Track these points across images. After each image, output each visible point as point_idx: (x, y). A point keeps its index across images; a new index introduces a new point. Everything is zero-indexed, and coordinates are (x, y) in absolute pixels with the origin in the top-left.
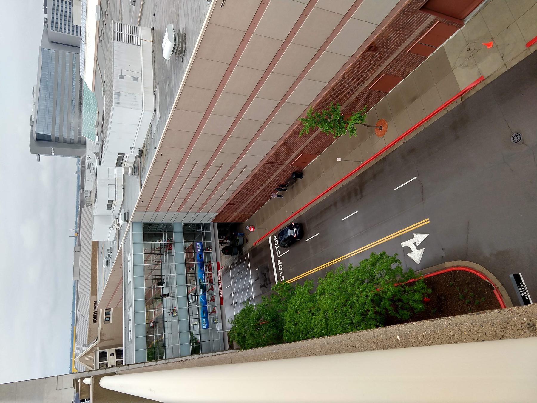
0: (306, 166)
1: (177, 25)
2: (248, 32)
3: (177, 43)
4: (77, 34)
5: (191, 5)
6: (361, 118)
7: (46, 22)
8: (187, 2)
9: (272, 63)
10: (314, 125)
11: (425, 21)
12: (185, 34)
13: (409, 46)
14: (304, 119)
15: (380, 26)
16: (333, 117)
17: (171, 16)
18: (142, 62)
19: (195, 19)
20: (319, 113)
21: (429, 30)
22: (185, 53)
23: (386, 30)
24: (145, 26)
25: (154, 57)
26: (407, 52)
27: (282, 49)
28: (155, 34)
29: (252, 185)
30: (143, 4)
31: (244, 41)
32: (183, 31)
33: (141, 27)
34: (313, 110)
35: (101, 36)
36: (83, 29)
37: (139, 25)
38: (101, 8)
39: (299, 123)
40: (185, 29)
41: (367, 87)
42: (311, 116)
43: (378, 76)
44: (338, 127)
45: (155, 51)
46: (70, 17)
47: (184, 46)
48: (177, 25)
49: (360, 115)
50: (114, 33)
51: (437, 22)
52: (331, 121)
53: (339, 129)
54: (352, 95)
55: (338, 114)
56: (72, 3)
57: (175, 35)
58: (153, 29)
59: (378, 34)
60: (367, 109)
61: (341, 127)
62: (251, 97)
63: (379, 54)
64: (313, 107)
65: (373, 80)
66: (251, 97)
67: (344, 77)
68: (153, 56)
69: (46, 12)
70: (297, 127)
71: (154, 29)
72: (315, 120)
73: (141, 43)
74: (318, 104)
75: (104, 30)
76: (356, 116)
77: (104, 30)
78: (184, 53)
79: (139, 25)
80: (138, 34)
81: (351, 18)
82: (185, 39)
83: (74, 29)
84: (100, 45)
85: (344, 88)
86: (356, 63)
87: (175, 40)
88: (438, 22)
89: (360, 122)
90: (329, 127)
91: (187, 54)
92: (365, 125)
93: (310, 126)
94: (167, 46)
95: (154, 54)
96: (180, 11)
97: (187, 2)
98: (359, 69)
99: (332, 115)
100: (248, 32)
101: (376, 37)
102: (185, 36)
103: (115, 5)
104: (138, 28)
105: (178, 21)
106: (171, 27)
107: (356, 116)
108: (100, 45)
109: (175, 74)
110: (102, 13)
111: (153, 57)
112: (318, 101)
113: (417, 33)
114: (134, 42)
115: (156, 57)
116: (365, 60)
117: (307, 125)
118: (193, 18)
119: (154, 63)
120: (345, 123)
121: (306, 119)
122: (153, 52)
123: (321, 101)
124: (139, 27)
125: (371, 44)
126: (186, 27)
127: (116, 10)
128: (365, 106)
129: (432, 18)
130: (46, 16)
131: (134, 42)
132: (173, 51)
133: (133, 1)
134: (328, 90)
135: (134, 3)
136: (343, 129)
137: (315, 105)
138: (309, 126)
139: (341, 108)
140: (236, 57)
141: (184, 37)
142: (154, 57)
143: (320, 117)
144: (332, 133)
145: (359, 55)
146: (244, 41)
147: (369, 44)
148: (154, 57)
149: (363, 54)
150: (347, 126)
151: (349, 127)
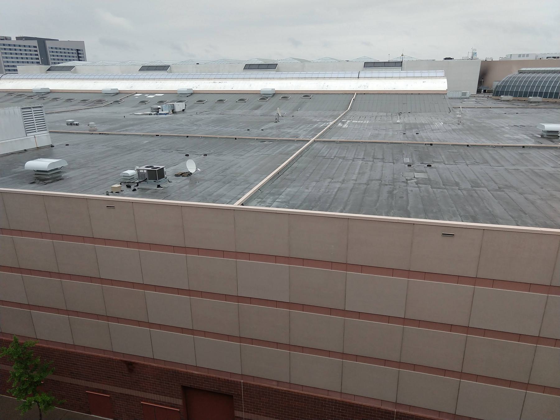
0: (93, 414)
1: (69, 169)
2: (93, 240)
3: (49, 173)
4: (6, 70)
5: (95, 178)
6: (48, 405)
7: (6, 38)
8: (96, 173)
9: (71, 276)
10: (14, 357)
11: (143, 392)
12: (63, 179)
13: (147, 400)
14: (17, 342)
15: (197, 368)
16: (35, 373)
17: (75, 161)
18: (7, 141)
19: (83, 184)
20: (32, 355)
21: (169, 407)
22: (41, 184)
23: (152, 367)
24: (51, 137)
25: (20, 153)
26: (141, 402)
27: (91, 279)
28: (48, 150)
29: (45, 360)
30: (74, 133)
31: (84, 239)
32: (66, 176)
33: (49, 134)
34: (34, 346)
35: (17, 95)
36: (13, 76)
37: (50, 132)
38: (49, 93)
39: (7, 339)
40: (68, 177)
41: (87, 388)
42: (25, 348)
43: (105, 392)
44: (24, 387)
45: (27, 152)
46: (23, 62)
47: (50, 181)
48: (69, 169)
49: (51, 402)
50: (29, 108)
51: (177, 409)
52: (28, 374)
53: (23, 389)
54: (71, 378)
55: (41, 377)
56: (39, 64)
57: (57, 169)
58: (52, 146)
59: (145, 363)
60: (63, 405)
61: (26, 389)
62: (20, 270)
63: (128, 376)
64: (37, 344)
65: (98, 389)
66: (20, 270)
67: (89, 356)
68: (22, 151)
69: (18, 38)
70: (2, 340)
71: (53, 148)
72: (22, 355)
73: (31, 136)
74: (43, 348)
75: (25, 97)
76: (48, 398)
77: (25, 97)
78: (41, 183)
79: (50, 132)
80: (39, 132)
81: (193, 336)
82: (58, 180)
83: (11, 67)
84: (5, 94)
85: (77, 365)
86: (110, 360)
87: (51, 171)
88: (179, 410)
89: (42, 407)
90: (20, 377)
91: (42, 185)
92: (41, 415)
93: (11, 354)
94: (43, 164)
95: (24, 152)
96: (83, 169)
97: (96, 173)
98: (104, 367)
99: (36, 371)
100: (93, 240)
101: (143, 362)
102: (61, 179)
103: (58, 106)
104: (45, 131)
105: (73, 169)
106: (65, 164)
107: (48, 398)
108: (5, 94)
109: (11, 179)
110: (43, 94)
111: (19, 152)
112: (47, 346)
113: (163, 398)
114: (28, 130)
115: (21, 155)
116: (116, 367)
117: (11, 349)
118: (84, 183)
119: (12, 154)
120: (33, 392)
121: (19, 344)
122: (25, 150)
123: (49, 349)
124: (47, 132)
125: (134, 363)
126: (71, 178)
127: (54, 108)
128: (65, 401)
129: (180, 402)
130: (14, 39)
131: (28, 130)
132: (38, 171)
133: (71, 123)
134: (65, 349)
135: (69, 125)
136: (24, 395)
137: (40, 345)
138: (9, 353)
139: (50, 376)
140: (62, 237)
141: (58, 178)
142: (20, 152)
143: (28, 358)
144: (13, 384)
145: (118, 358)
146: (84, 239)
147: (133, 361)
148: (20, 153)
149: (121, 360)
150: (30, 396)
151: (30, 398)
